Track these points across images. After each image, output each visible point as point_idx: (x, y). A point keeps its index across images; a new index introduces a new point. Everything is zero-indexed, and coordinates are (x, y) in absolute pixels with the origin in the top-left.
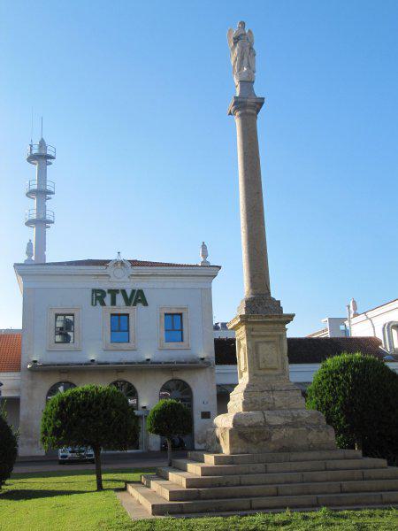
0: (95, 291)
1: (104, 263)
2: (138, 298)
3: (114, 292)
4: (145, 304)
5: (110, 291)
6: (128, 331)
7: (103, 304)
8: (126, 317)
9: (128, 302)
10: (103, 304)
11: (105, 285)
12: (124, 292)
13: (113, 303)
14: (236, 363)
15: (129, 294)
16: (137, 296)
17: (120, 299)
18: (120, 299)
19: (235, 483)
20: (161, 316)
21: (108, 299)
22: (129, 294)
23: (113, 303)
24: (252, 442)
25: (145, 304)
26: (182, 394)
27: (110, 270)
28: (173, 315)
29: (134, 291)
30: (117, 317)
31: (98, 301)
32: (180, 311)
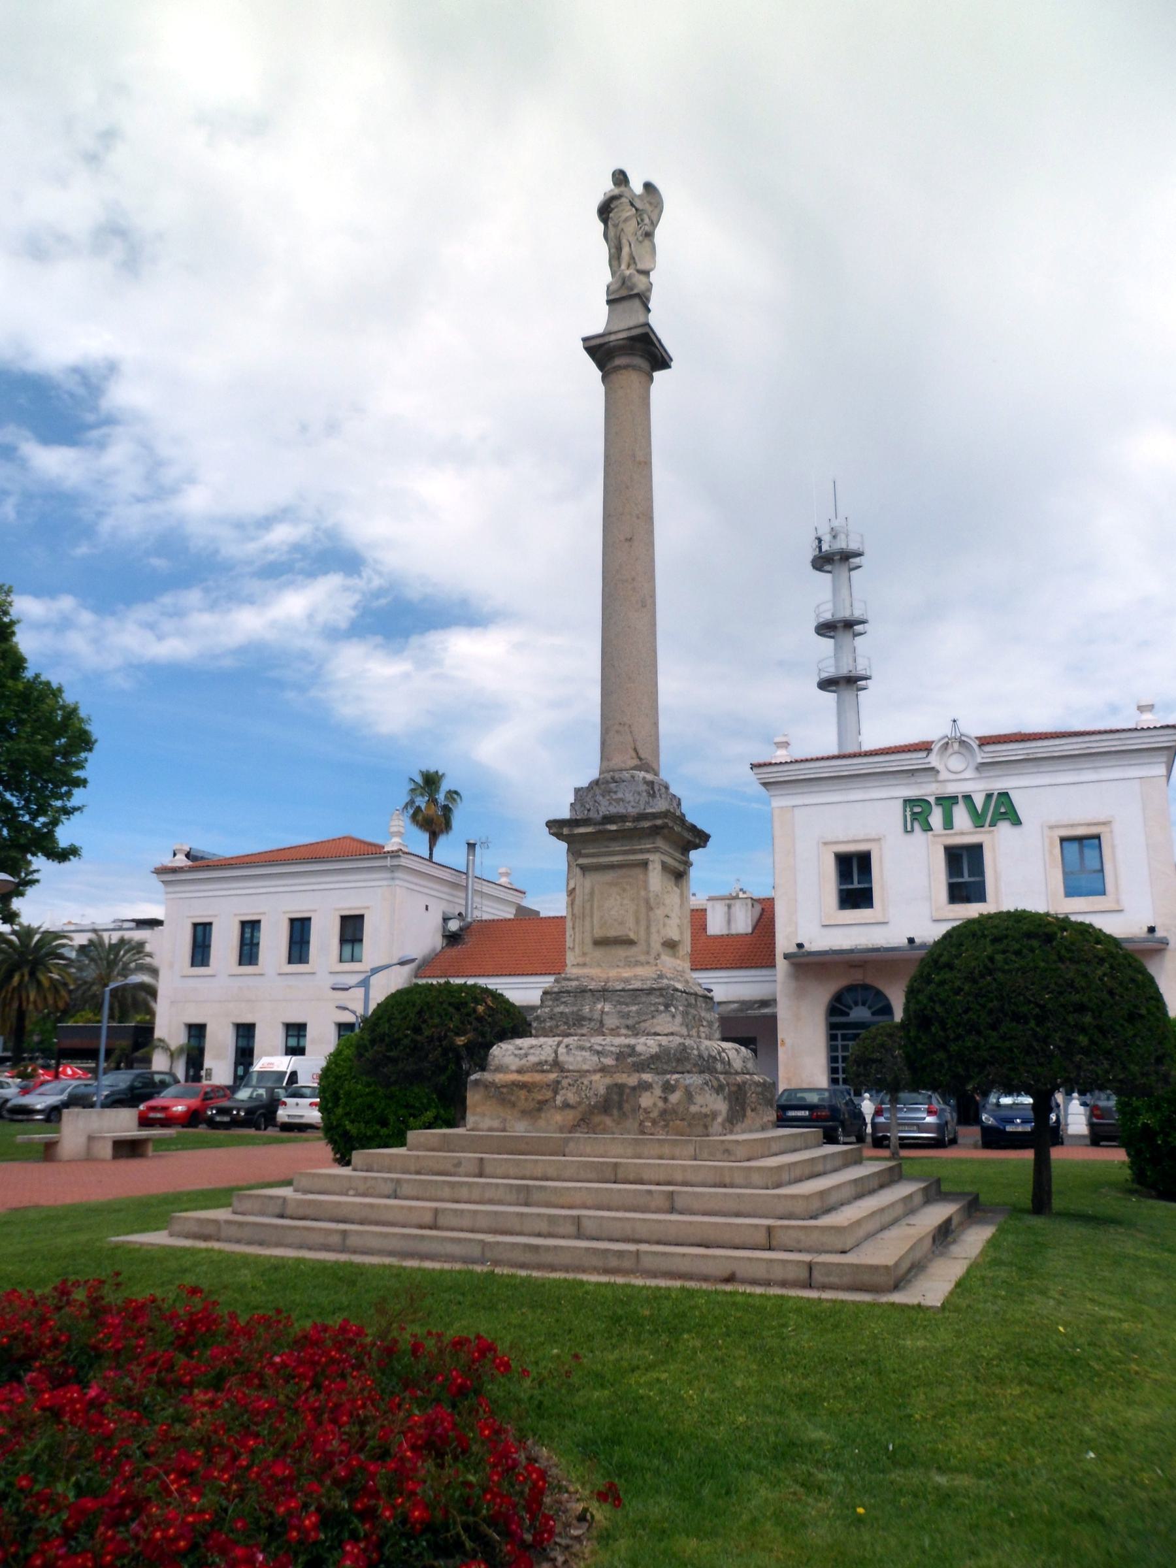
0: (908, 802)
1: (925, 747)
2: (1003, 809)
3: (947, 802)
4: (1017, 822)
5: (940, 800)
6: (1102, 870)
7: (928, 828)
8: (1096, 841)
9: (978, 819)
10: (928, 828)
11: (927, 790)
12: (968, 798)
13: (948, 823)
14: (774, 966)
15: (979, 801)
16: (997, 807)
17: (960, 815)
18: (960, 815)
19: (539, 1175)
20: (1051, 844)
21: (936, 818)
22: (979, 801)
23: (948, 823)
24: (514, 1105)
25: (1017, 822)
26: (873, 1014)
27: (934, 760)
28: (1080, 839)
29: (989, 796)
30: (1075, 846)
31: (917, 826)
32: (1093, 830)
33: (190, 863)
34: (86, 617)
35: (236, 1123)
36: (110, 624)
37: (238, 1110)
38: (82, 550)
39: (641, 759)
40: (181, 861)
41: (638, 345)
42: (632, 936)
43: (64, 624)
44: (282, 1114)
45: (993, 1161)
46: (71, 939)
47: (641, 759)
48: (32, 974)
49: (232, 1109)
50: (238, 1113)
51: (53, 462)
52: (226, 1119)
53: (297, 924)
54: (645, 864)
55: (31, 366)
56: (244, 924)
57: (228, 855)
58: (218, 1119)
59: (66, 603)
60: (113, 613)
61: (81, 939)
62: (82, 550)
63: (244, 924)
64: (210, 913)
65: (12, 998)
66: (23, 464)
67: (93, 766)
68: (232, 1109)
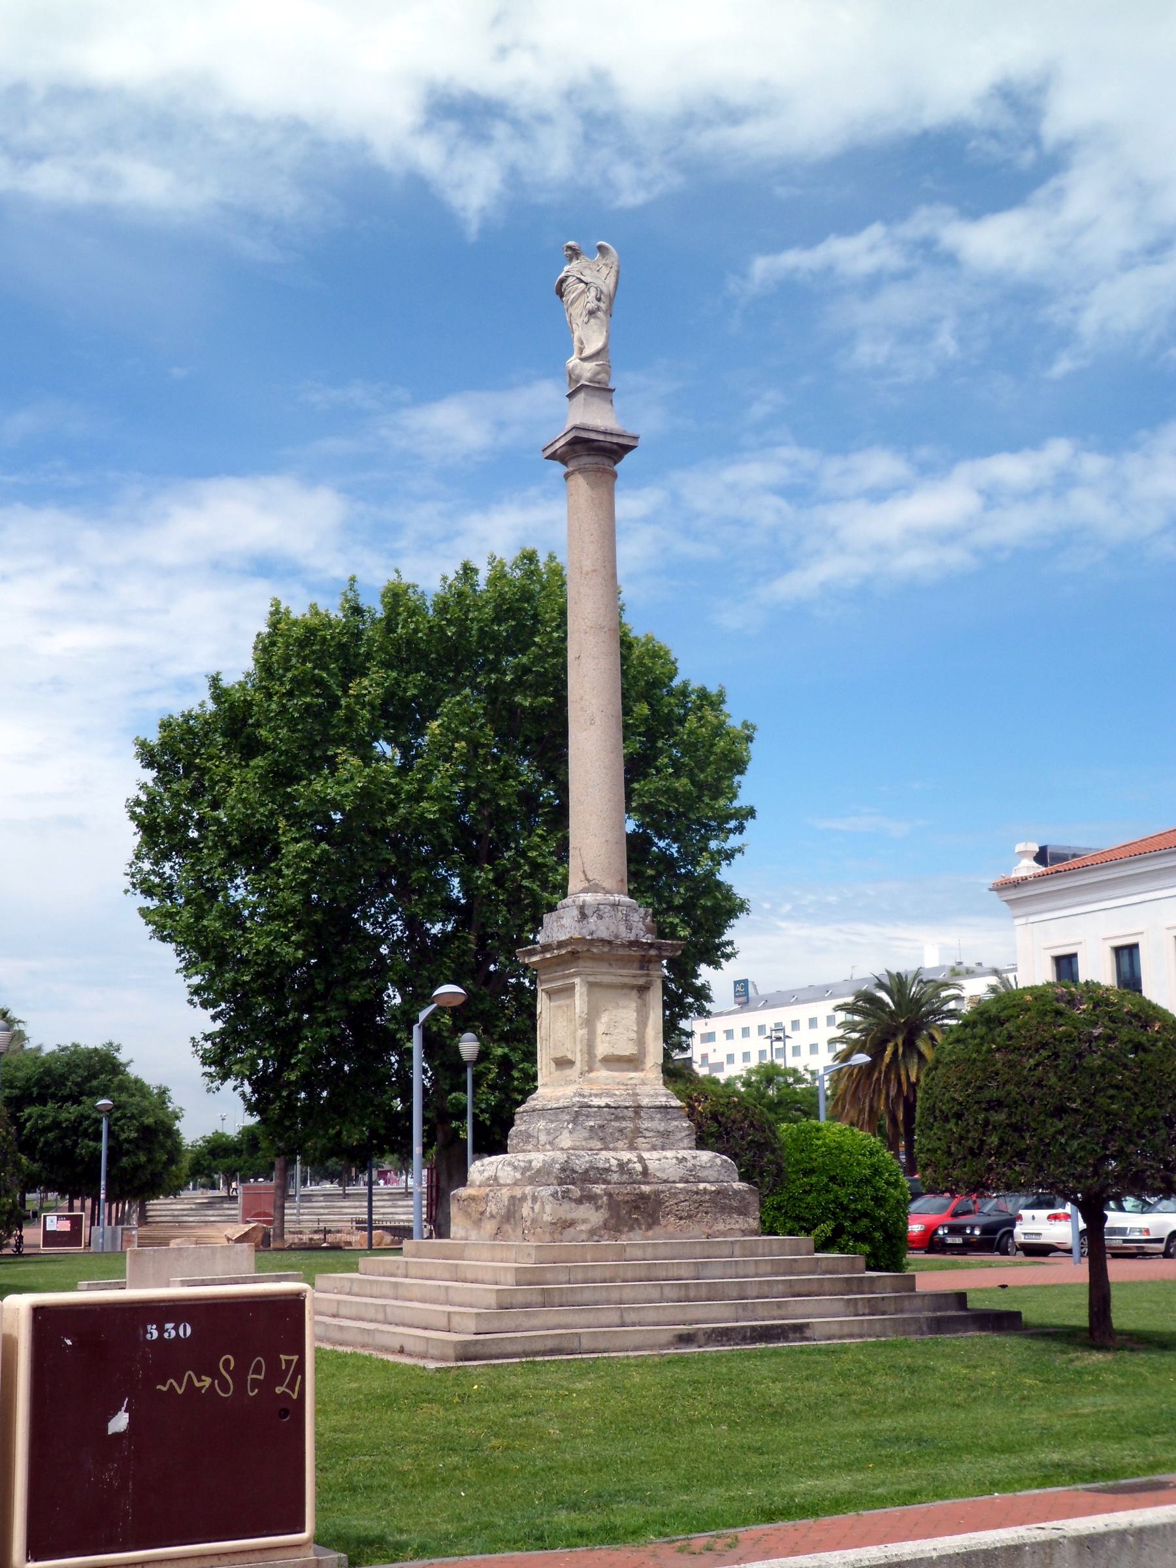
33: (1041, 869)
34: (1093, 464)
35: (968, 1247)
36: (1132, 464)
37: (973, 1229)
38: (1063, 365)
39: (589, 881)
40: (1027, 867)
41: (578, 447)
42: (570, 1056)
43: (1064, 482)
44: (1020, 1232)
45: (927, 1260)
46: (961, 988)
47: (589, 881)
48: (910, 1043)
49: (964, 1227)
50: (972, 1233)
51: (996, 242)
52: (959, 1240)
53: (1064, 962)
54: (572, 987)
55: (933, 116)
56: (1118, 950)
57: (1107, 847)
58: (950, 1240)
59: (1059, 451)
60: (1134, 447)
61: (976, 988)
62: (1063, 365)
63: (1118, 950)
64: (1073, 940)
65: (887, 1081)
66: (950, 260)
67: (749, 789)
68: (964, 1227)
